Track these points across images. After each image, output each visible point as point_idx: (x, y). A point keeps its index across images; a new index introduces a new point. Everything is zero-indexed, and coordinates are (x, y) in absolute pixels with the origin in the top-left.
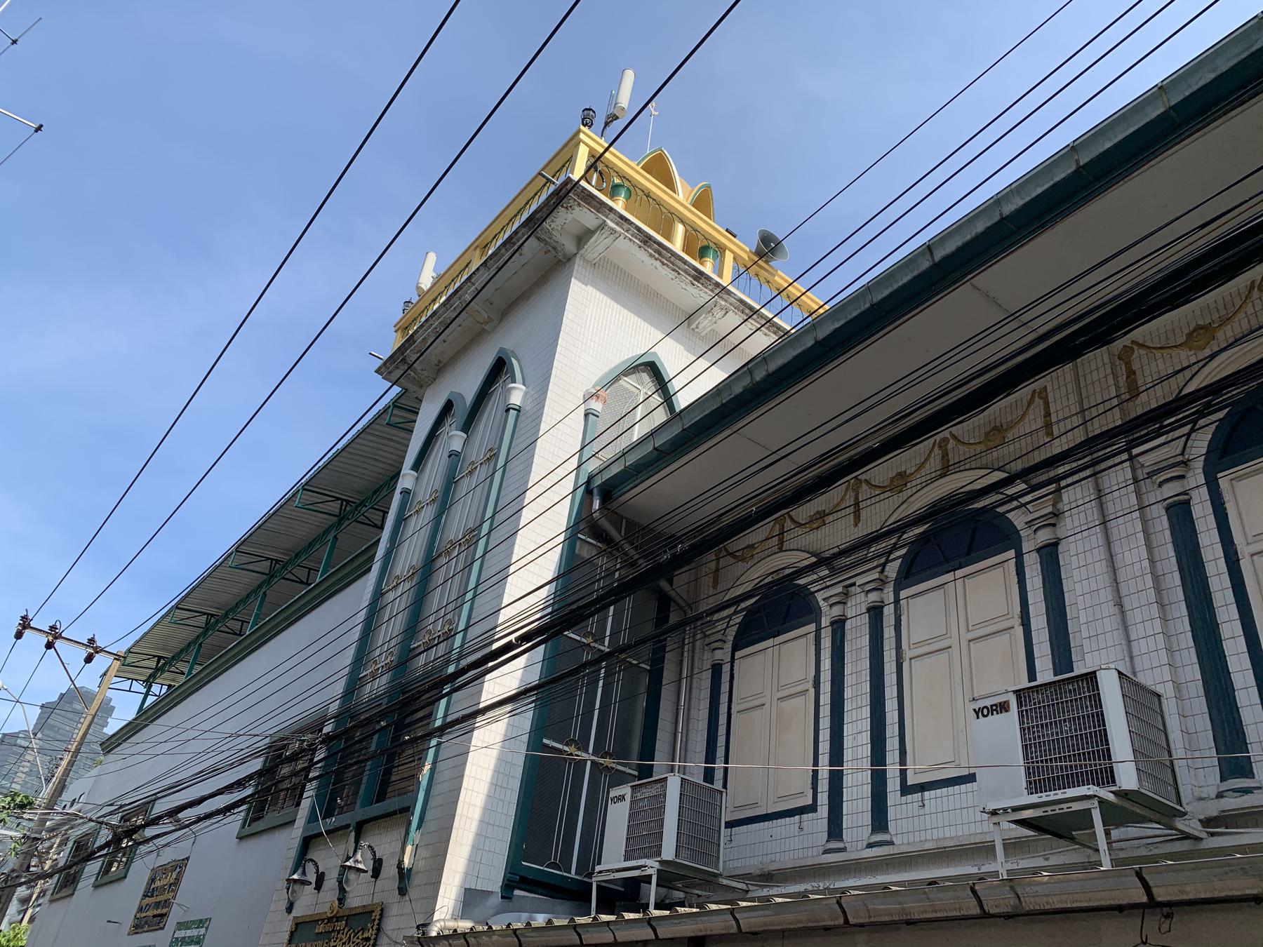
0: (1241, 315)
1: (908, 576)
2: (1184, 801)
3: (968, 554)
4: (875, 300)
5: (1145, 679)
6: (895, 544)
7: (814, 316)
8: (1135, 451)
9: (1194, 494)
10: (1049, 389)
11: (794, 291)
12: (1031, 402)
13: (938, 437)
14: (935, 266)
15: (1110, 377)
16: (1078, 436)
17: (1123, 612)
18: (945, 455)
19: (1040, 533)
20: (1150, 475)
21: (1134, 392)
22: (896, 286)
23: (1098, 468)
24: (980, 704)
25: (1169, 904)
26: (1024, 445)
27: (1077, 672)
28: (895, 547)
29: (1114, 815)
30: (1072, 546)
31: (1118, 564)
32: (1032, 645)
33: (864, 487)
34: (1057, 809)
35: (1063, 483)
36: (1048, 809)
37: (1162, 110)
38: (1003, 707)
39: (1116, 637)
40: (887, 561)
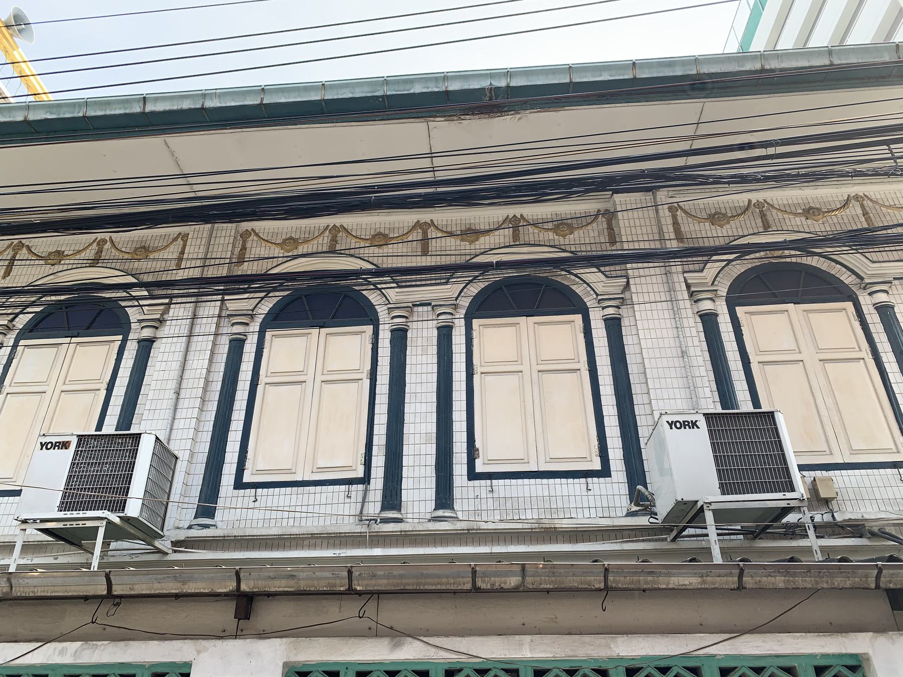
0: (315, 242)
1: (33, 330)
2: (165, 528)
3: (88, 328)
4: (88, 114)
5: (173, 447)
6: (34, 302)
7: (37, 98)
8: (226, 297)
9: (250, 337)
10: (190, 236)
11: (27, 69)
12: (175, 239)
13: (100, 236)
14: (143, 114)
15: (230, 246)
16: (196, 273)
17: (177, 399)
18: (100, 251)
19: (145, 330)
20: (229, 316)
21: (241, 261)
22: (108, 112)
23: (200, 299)
24: (48, 439)
25: (120, 597)
26: (159, 265)
27: (132, 431)
28: (32, 304)
29: (113, 532)
30: (163, 346)
31: (188, 367)
32: (375, 394)
33: (24, 250)
34: (68, 525)
35: (175, 300)
36: (68, 523)
37: (318, 98)
38: (65, 445)
39: (168, 414)
40: (21, 313)
